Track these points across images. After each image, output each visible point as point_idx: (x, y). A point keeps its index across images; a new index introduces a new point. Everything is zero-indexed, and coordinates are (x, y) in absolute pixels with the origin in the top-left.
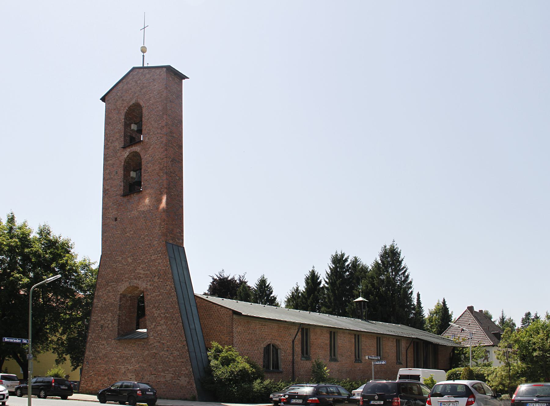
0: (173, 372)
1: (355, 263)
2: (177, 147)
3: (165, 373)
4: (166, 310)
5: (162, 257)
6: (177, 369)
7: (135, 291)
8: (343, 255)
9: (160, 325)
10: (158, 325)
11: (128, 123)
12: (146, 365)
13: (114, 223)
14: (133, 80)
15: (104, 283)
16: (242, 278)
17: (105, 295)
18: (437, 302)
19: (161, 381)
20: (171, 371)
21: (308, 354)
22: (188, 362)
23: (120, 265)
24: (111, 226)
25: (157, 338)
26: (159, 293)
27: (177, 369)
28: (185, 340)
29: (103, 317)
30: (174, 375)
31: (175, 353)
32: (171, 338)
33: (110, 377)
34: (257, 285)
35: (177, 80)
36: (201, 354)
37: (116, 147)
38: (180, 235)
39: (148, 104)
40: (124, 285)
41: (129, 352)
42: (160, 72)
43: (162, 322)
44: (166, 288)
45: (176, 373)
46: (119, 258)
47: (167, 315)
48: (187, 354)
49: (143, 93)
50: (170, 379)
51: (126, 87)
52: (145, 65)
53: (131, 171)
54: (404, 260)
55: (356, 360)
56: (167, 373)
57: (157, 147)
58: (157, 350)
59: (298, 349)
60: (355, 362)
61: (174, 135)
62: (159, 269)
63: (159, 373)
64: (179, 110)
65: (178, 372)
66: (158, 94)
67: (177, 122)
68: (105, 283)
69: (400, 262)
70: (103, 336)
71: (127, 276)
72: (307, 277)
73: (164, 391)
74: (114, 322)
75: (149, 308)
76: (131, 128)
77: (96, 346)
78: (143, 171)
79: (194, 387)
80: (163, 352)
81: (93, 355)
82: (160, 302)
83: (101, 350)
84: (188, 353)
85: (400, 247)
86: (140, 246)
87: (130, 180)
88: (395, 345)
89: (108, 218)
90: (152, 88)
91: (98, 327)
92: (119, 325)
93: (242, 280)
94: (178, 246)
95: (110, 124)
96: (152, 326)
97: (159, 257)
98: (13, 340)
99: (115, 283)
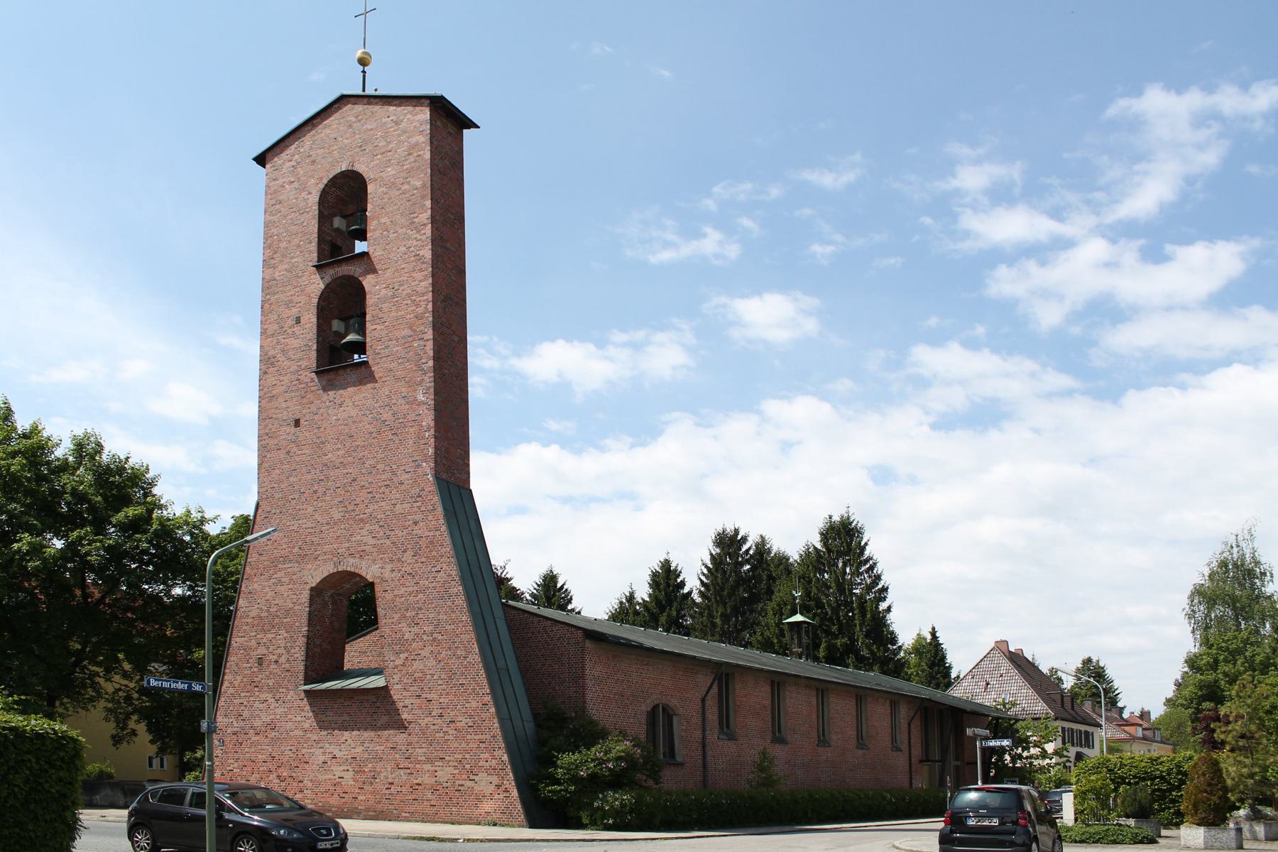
1: (762, 548)
2: (454, 271)
6: (467, 756)
7: (344, 583)
8: (737, 531)
11: (326, 213)
12: (382, 748)
13: (293, 430)
15: (266, 563)
16: (501, 571)
18: (918, 632)
19: (425, 782)
21: (731, 728)
25: (411, 689)
27: (467, 756)
29: (264, 640)
33: (285, 774)
34: (538, 585)
35: (452, 129)
36: (523, 724)
38: (462, 462)
41: (335, 718)
44: (437, 577)
45: (464, 766)
47: (440, 637)
54: (869, 543)
55: (819, 741)
59: (713, 716)
60: (818, 745)
61: (448, 245)
64: (458, 192)
65: (470, 764)
67: (453, 217)
69: (863, 549)
72: (652, 571)
74: (293, 651)
76: (332, 226)
77: (245, 703)
78: (368, 317)
80: (430, 719)
85: (858, 519)
87: (331, 339)
88: (889, 711)
93: (499, 574)
94: (459, 486)
98: (170, 685)
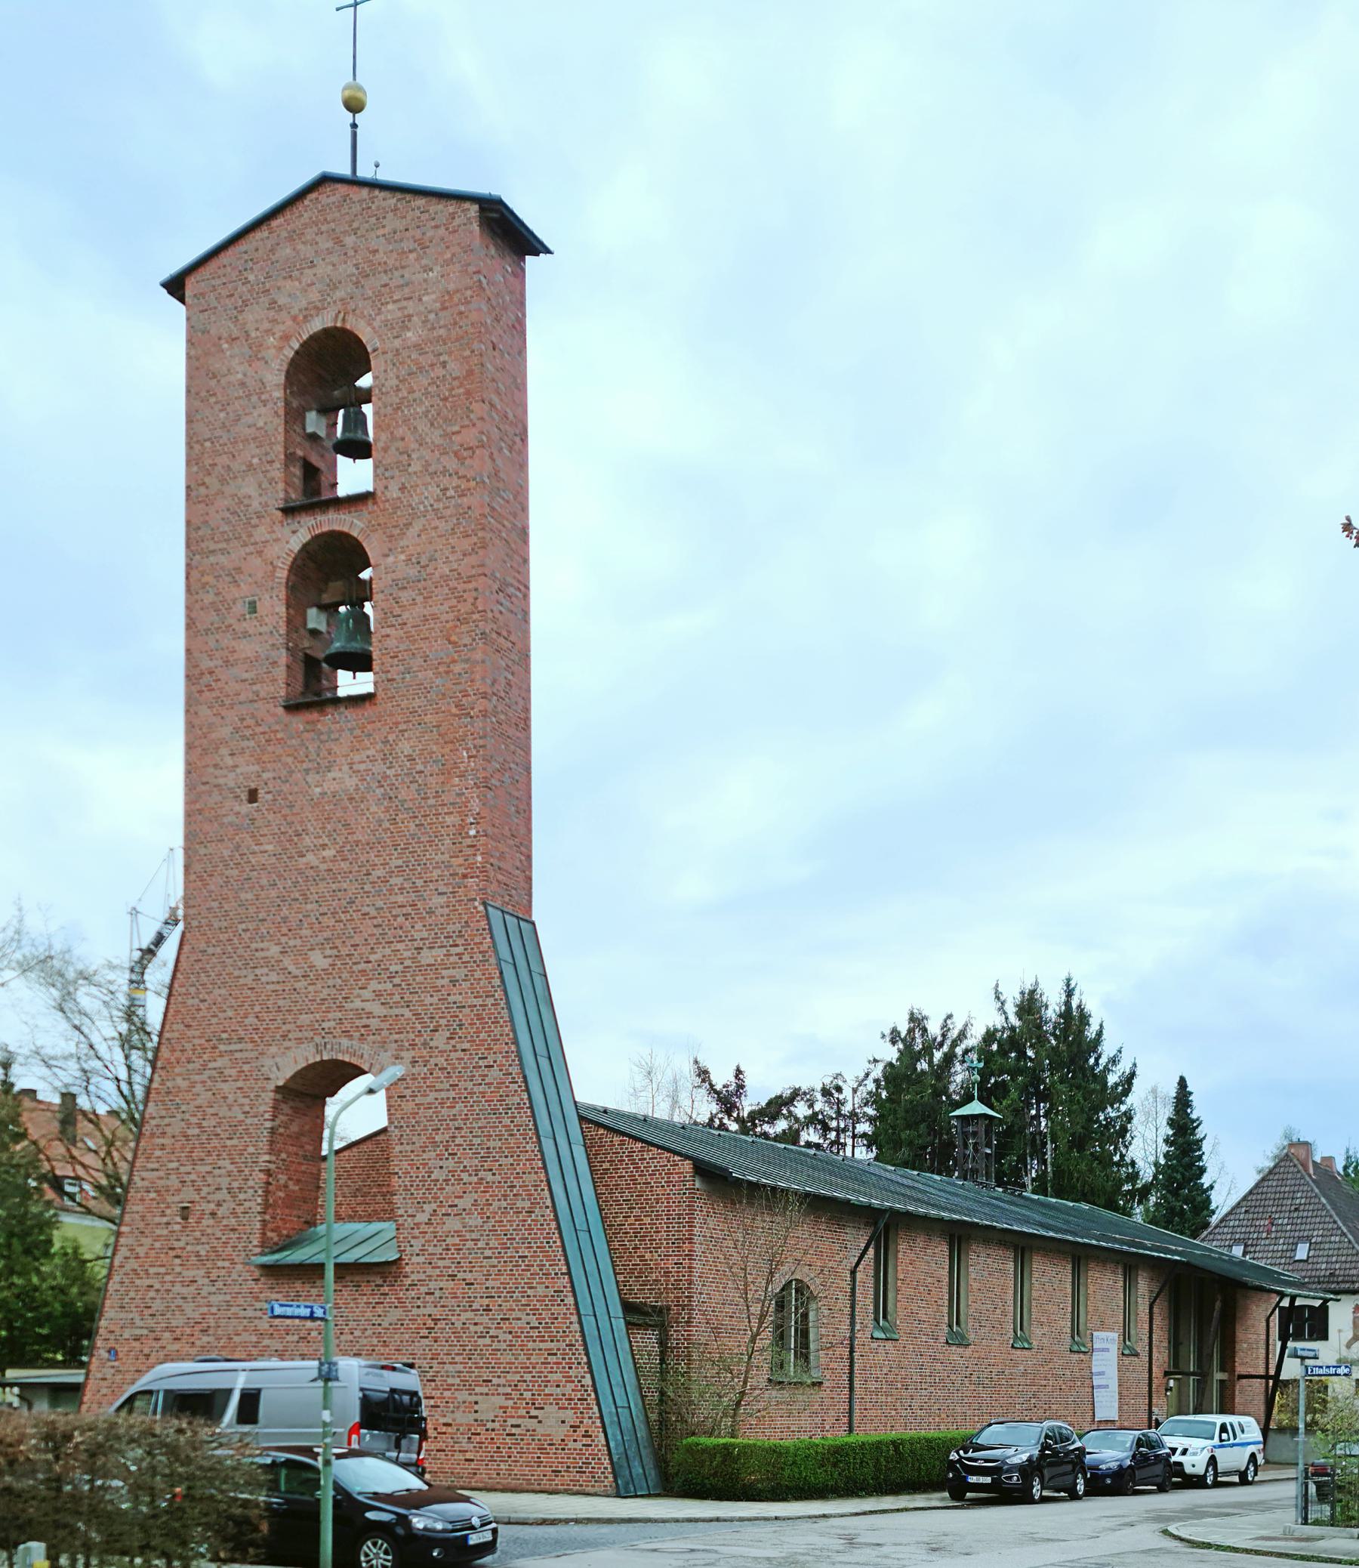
0: (508, 1390)
3: (476, 1394)
4: (484, 1159)
5: (466, 958)
9: (455, 1215)
10: (449, 1215)
13: (246, 808)
14: (324, 228)
17: (199, 1088)
20: (499, 1385)
22: (574, 1354)
23: (274, 977)
24: (231, 818)
25: (441, 1263)
26: (452, 1094)
28: (564, 1271)
29: (193, 1177)
30: (513, 1399)
31: (519, 1319)
32: (505, 1262)
37: (246, 502)
39: (397, 343)
40: (291, 1054)
42: (453, 216)
43: (465, 1203)
44: (487, 1076)
45: (521, 1394)
46: (268, 950)
48: (571, 1323)
49: (370, 293)
50: (496, 1416)
51: (288, 251)
52: (365, 172)
53: (311, 606)
56: (482, 1394)
57: (443, 526)
58: (443, 1306)
62: (455, 1003)
63: (447, 1394)
66: (444, 308)
68: (203, 1041)
70: (189, 1248)
71: (305, 1019)
73: (466, 1460)
75: (409, 1148)
76: (304, 429)
79: (597, 1446)
80: (470, 1315)
81: (139, 1323)
82: (456, 1129)
83: (180, 1302)
84: (574, 1318)
86: (366, 909)
89: (215, 786)
90: (414, 278)
91: (168, 1211)
92: (266, 1206)
94: (518, 918)
95: (213, 400)
96: (422, 1218)
97: (453, 959)
99: (250, 1046)
